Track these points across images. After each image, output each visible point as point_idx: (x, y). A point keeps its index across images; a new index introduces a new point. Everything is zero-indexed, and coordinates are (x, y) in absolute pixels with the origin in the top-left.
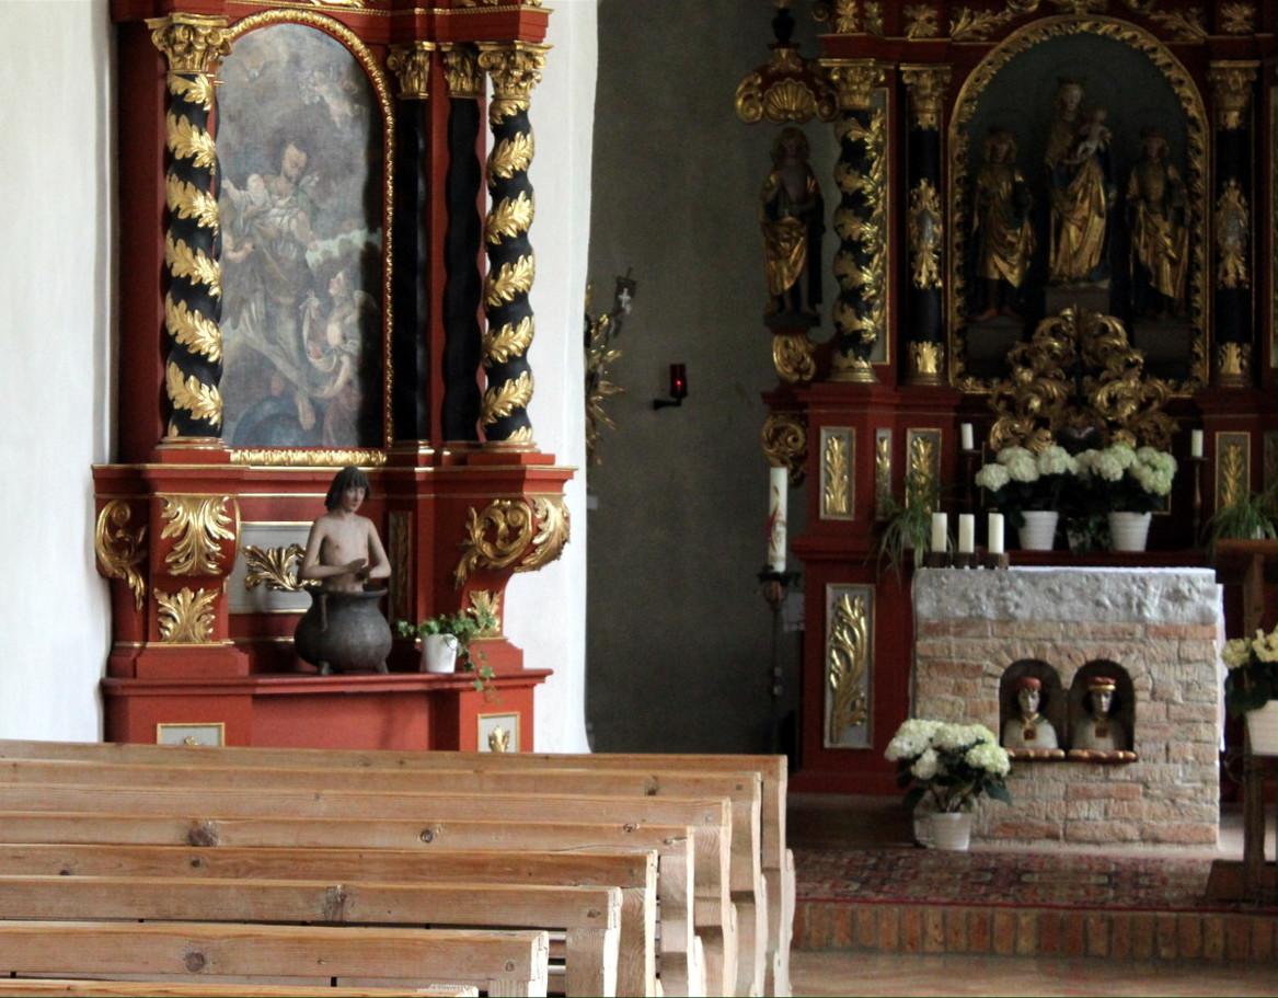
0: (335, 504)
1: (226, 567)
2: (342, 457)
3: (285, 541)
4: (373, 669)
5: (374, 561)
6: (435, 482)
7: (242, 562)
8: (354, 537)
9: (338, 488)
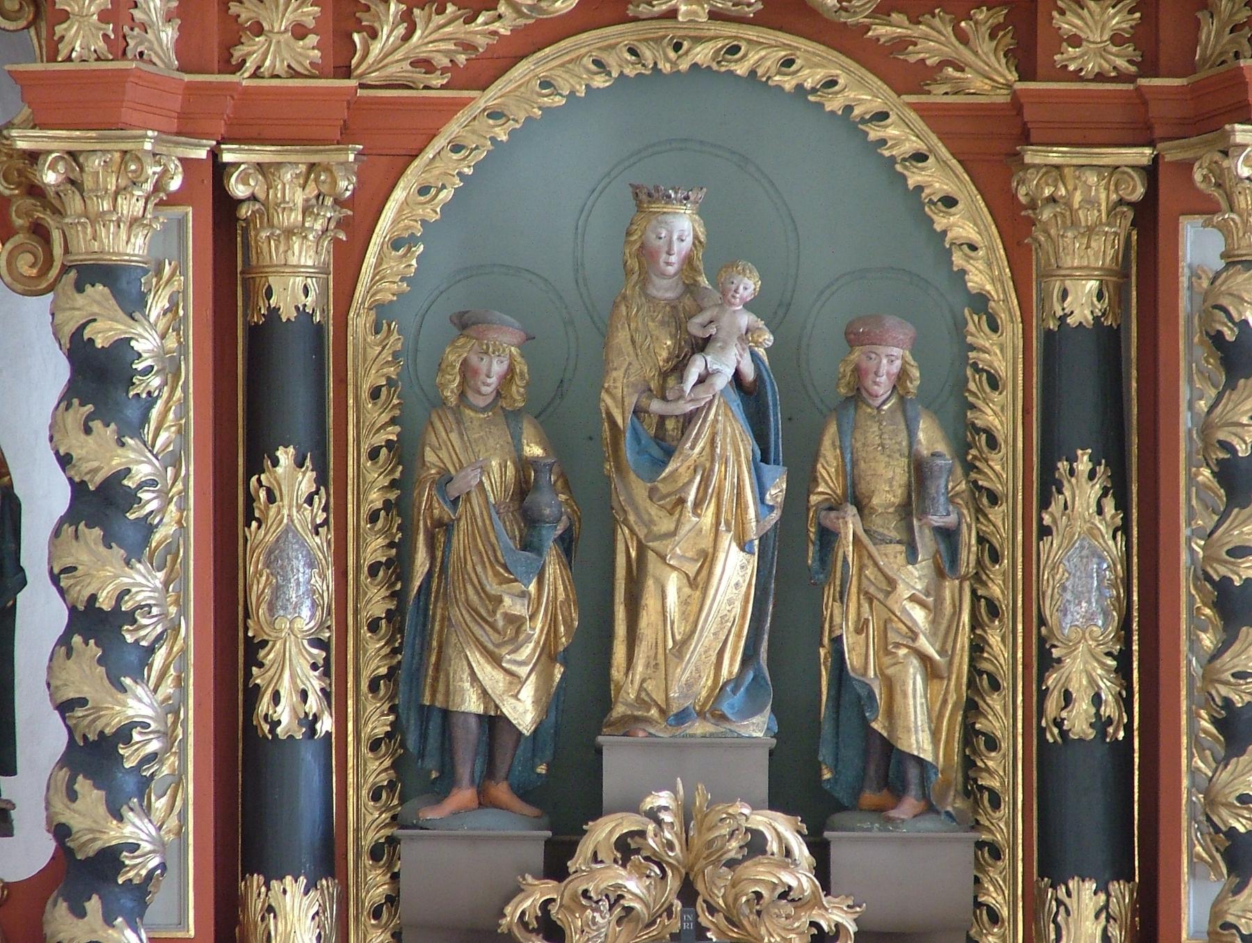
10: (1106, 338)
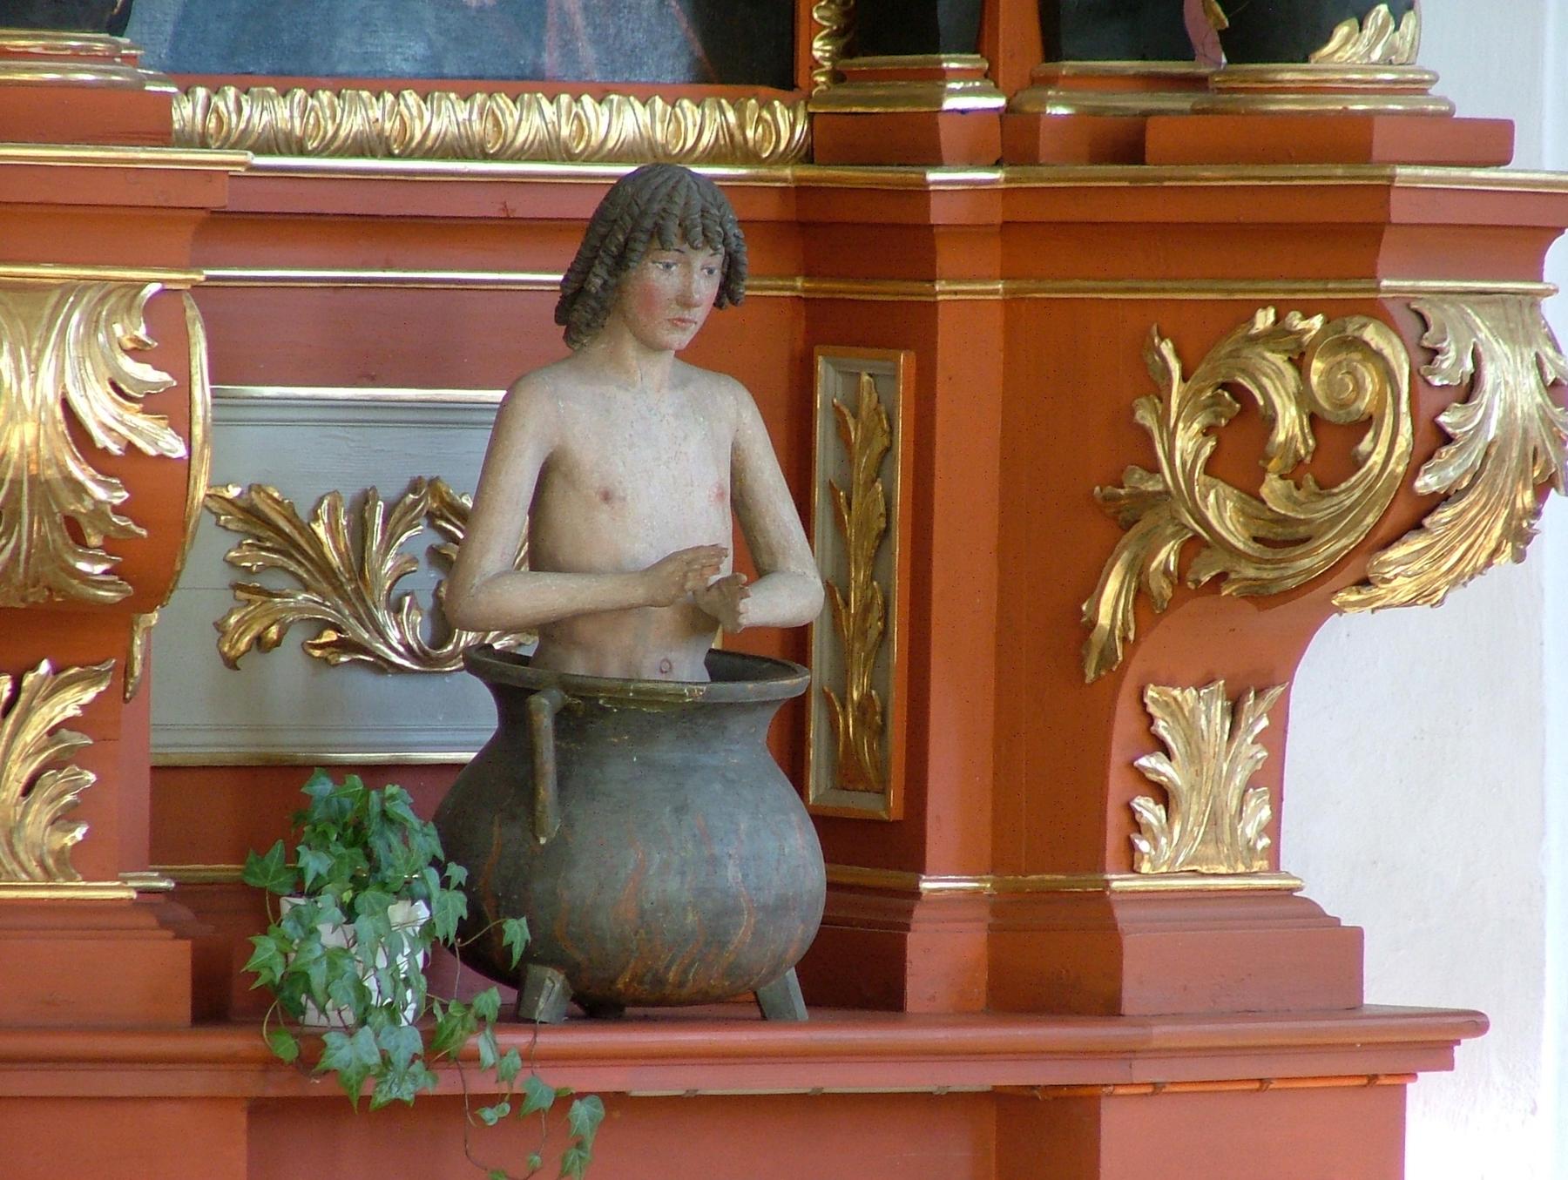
0: (588, 309)
1: (149, 581)
2: (623, 121)
3: (391, 463)
4: (742, 1001)
5: (753, 557)
6: (1018, 231)
7: (211, 554)
8: (663, 458)
9: (605, 247)
10: (107, 538)
